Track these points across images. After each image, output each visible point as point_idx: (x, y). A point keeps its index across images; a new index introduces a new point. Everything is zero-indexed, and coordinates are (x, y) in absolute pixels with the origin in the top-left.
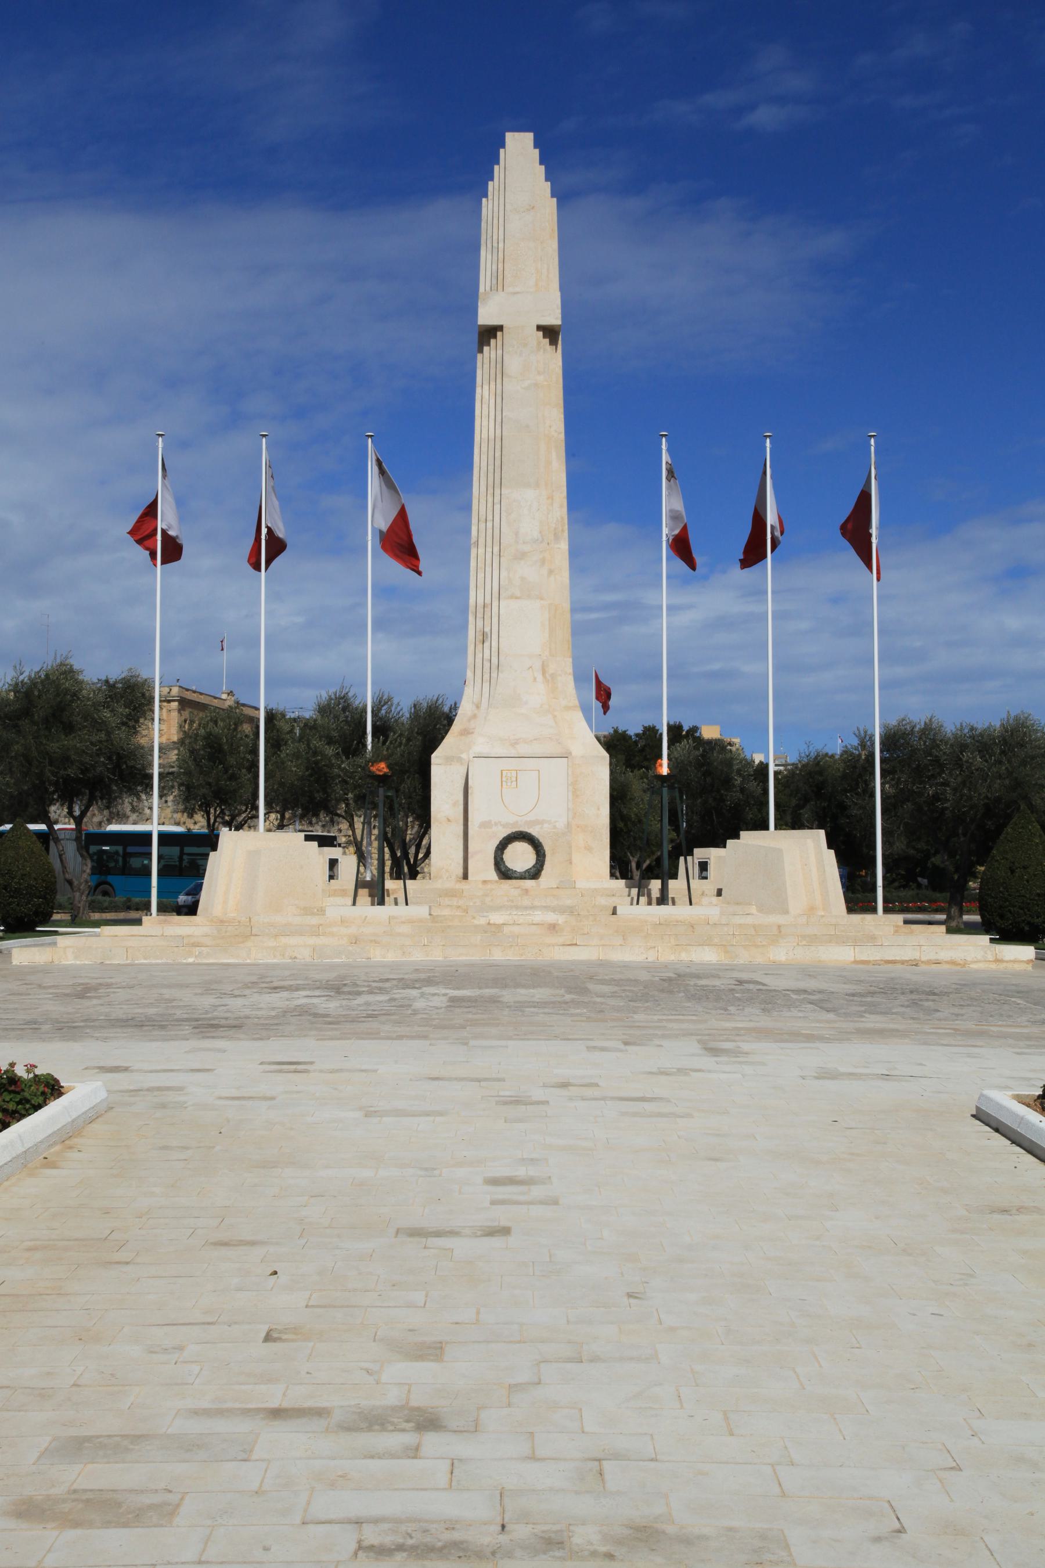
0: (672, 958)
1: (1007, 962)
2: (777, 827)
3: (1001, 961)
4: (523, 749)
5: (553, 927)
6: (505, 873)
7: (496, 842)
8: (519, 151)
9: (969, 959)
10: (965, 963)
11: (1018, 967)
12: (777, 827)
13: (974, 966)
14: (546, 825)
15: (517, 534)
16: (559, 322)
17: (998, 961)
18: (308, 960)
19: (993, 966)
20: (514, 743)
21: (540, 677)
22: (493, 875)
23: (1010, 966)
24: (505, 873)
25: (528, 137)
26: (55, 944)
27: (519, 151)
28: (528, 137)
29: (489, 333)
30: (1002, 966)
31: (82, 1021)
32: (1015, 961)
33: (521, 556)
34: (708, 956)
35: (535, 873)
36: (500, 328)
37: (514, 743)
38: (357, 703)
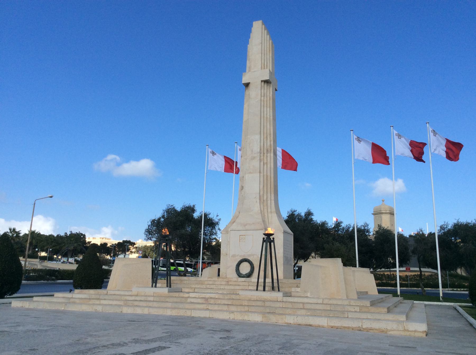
0: (241, 318)
1: (411, 331)
2: (434, 234)
3: (408, 331)
4: (247, 227)
5: (206, 299)
6: (249, 275)
7: (236, 263)
8: (258, 28)
9: (389, 328)
10: (387, 330)
11: (417, 335)
12: (434, 234)
13: (390, 333)
14: (255, 256)
15: (252, 151)
16: (268, 78)
17: (405, 330)
18: (101, 311)
19: (403, 333)
20: (245, 225)
21: (258, 201)
22: (235, 275)
23: (412, 334)
24: (240, 275)
25: (260, 22)
26: (53, 295)
27: (258, 28)
28: (260, 22)
29: (247, 85)
30: (408, 334)
31: (48, 326)
32: (415, 331)
33: (253, 158)
34: (257, 318)
35: (249, 275)
36: (249, 83)
37: (245, 225)
38: (330, 225)
